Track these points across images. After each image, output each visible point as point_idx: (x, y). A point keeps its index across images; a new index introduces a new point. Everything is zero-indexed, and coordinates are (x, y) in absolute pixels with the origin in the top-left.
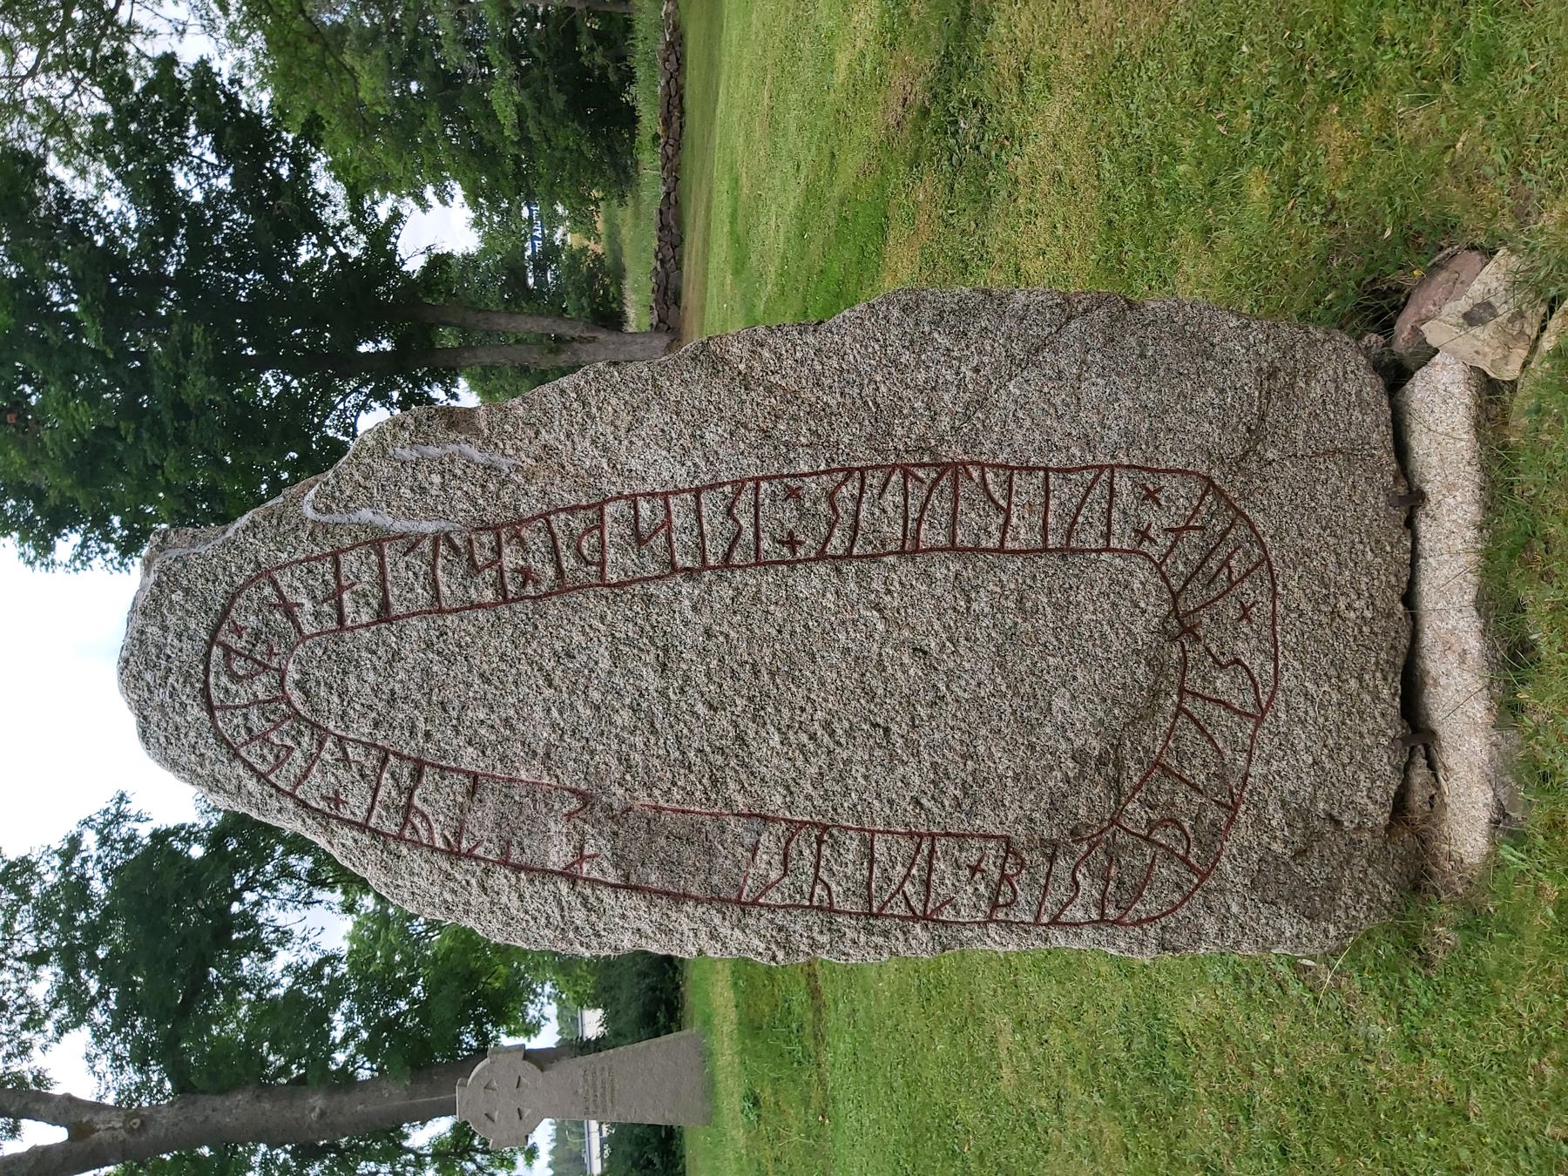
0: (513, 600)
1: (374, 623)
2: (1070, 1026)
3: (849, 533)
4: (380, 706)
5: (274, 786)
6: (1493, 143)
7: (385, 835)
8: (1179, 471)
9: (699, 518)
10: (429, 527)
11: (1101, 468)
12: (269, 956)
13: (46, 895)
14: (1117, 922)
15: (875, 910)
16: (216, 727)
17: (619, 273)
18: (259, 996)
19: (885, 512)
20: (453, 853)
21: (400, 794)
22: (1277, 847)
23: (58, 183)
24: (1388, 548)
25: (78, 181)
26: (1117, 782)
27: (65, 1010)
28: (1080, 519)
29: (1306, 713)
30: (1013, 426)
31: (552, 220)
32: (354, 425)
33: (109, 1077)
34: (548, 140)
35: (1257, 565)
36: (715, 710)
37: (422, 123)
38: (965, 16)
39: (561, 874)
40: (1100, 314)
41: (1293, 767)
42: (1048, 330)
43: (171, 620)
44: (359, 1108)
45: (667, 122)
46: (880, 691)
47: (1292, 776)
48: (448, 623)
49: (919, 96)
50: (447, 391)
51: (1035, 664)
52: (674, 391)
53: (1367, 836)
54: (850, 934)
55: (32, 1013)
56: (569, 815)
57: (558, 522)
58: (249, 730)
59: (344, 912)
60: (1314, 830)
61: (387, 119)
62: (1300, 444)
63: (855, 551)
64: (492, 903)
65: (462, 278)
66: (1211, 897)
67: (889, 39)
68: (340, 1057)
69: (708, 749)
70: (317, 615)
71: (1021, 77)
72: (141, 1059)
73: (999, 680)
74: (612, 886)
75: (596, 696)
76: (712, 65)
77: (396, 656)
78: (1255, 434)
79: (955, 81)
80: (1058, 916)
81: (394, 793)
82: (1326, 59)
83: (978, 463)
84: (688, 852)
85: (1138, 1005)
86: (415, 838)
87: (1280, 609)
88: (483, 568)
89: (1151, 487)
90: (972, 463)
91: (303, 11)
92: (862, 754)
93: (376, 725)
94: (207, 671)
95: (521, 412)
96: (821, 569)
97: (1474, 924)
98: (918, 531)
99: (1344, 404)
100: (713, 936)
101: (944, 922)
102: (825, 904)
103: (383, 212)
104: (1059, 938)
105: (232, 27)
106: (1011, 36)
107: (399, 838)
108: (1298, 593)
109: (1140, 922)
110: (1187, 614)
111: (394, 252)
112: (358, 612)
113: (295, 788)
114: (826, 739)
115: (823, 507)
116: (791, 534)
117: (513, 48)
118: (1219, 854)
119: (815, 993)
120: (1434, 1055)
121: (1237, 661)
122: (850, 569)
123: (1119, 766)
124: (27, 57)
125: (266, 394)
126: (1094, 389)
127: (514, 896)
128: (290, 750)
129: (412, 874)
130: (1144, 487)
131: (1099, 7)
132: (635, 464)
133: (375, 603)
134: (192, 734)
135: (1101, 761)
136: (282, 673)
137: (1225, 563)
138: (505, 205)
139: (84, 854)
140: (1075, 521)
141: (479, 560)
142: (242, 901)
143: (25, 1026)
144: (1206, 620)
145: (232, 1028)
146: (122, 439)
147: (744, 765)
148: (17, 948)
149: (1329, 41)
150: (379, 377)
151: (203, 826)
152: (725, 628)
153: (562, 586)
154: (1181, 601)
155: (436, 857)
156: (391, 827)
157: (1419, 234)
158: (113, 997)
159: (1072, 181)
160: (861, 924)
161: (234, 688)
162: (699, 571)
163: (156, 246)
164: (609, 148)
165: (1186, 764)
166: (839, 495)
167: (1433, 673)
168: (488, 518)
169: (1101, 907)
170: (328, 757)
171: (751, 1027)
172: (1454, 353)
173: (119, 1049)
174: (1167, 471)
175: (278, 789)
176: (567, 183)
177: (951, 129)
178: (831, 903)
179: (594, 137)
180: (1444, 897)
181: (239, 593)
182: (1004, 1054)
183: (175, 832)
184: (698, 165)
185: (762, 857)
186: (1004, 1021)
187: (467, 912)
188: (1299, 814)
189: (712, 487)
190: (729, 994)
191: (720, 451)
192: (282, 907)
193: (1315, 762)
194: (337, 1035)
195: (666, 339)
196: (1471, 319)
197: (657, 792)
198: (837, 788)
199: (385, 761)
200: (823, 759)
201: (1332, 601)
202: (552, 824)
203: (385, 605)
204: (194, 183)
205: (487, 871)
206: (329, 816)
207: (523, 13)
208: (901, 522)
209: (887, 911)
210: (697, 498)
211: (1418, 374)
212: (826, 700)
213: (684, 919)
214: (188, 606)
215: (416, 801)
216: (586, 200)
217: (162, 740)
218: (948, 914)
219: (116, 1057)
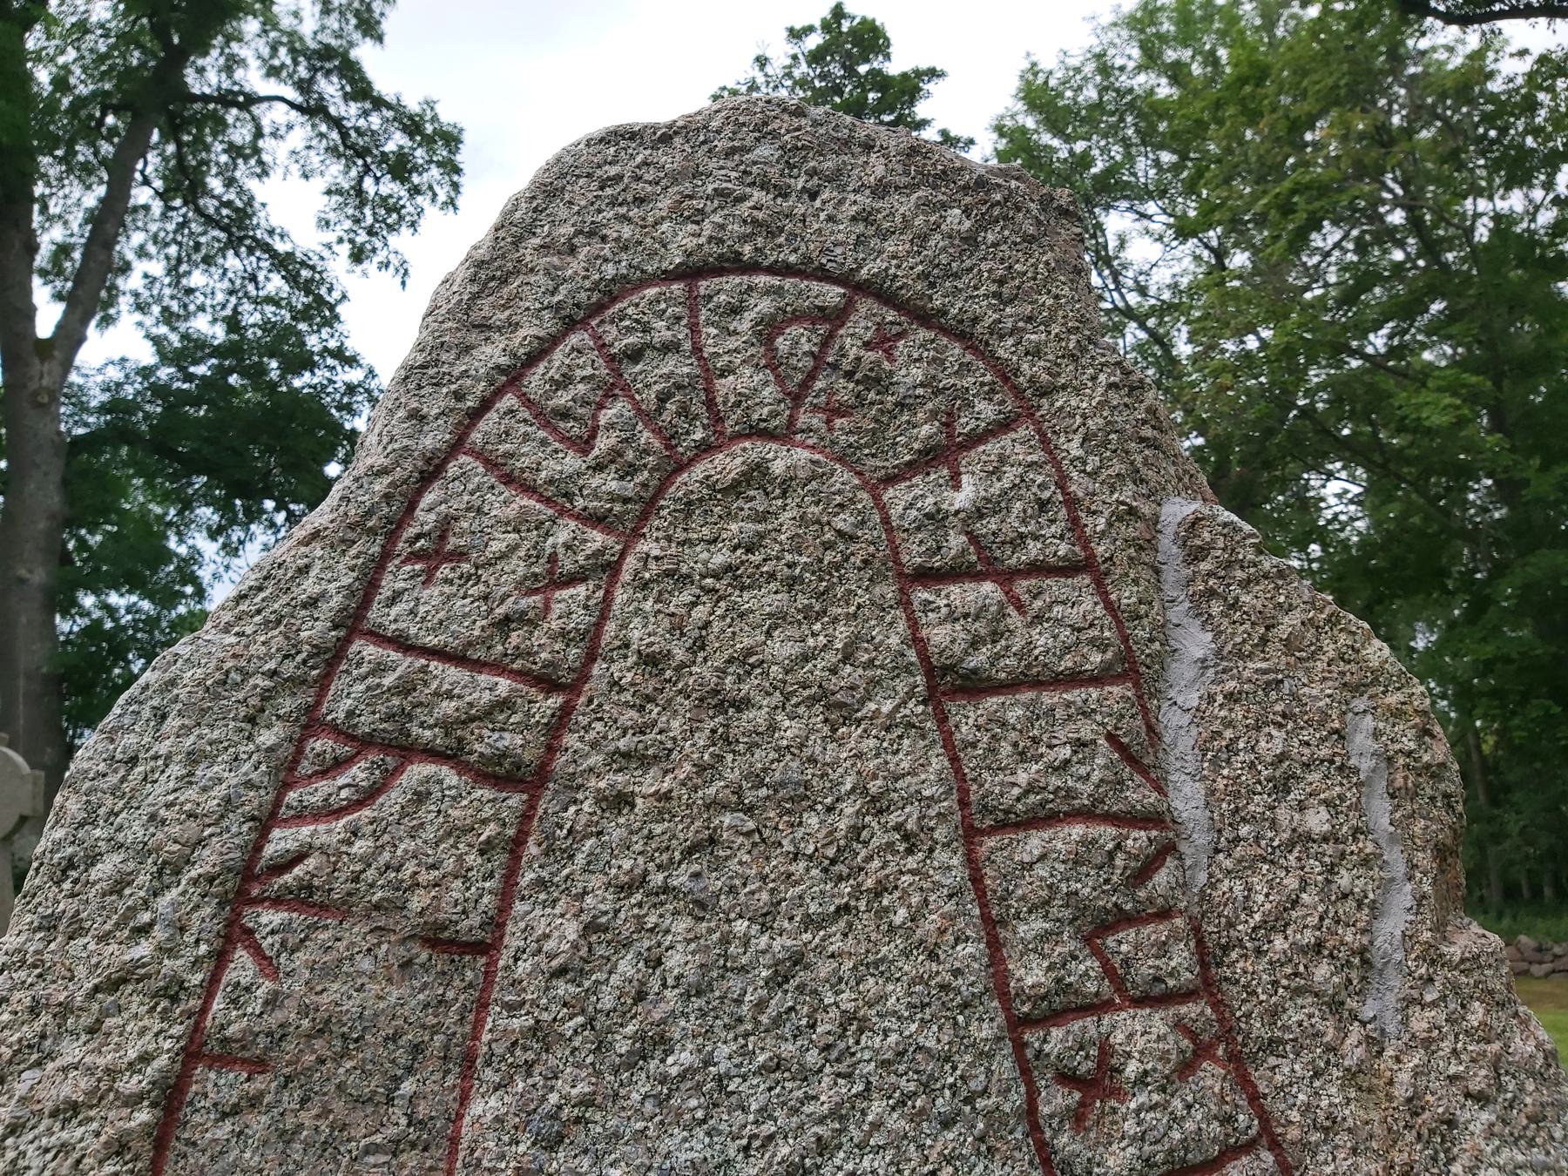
0: (1020, 1046)
1: (924, 657)
4: (703, 671)
5: (486, 405)
10: (1187, 799)
12: (213, 534)
13: (299, 334)
18: (170, 524)
20: (246, 882)
21: (446, 725)
27: (177, 344)
43: (903, 205)
44: (24, 620)
48: (941, 856)
55: (179, 316)
58: (635, 355)
64: (65, 1010)
68: (88, 601)
70: (936, 519)
72: (116, 406)
77: (841, 712)
81: (447, 707)
86: (306, 767)
88: (1097, 953)
93: (651, 661)
94: (785, 270)
107: (311, 722)
112: (952, 617)
113: (478, 455)
127: (74, 1088)
134: (627, 231)
136: (785, 435)
139: (339, 368)
141: (1123, 942)
142: (277, 509)
143: (166, 309)
145: (136, 498)
148: (247, 306)
155: (239, 829)
158: (186, 386)
161: (744, 324)
168: (1240, 966)
170: (562, 536)
181: (973, 349)
187: (49, 925)
194: (114, 599)
199: (547, 682)
203: (975, 686)
205: (173, 991)
214: (936, 240)
215: (418, 771)
217: (613, 171)
219: (119, 385)
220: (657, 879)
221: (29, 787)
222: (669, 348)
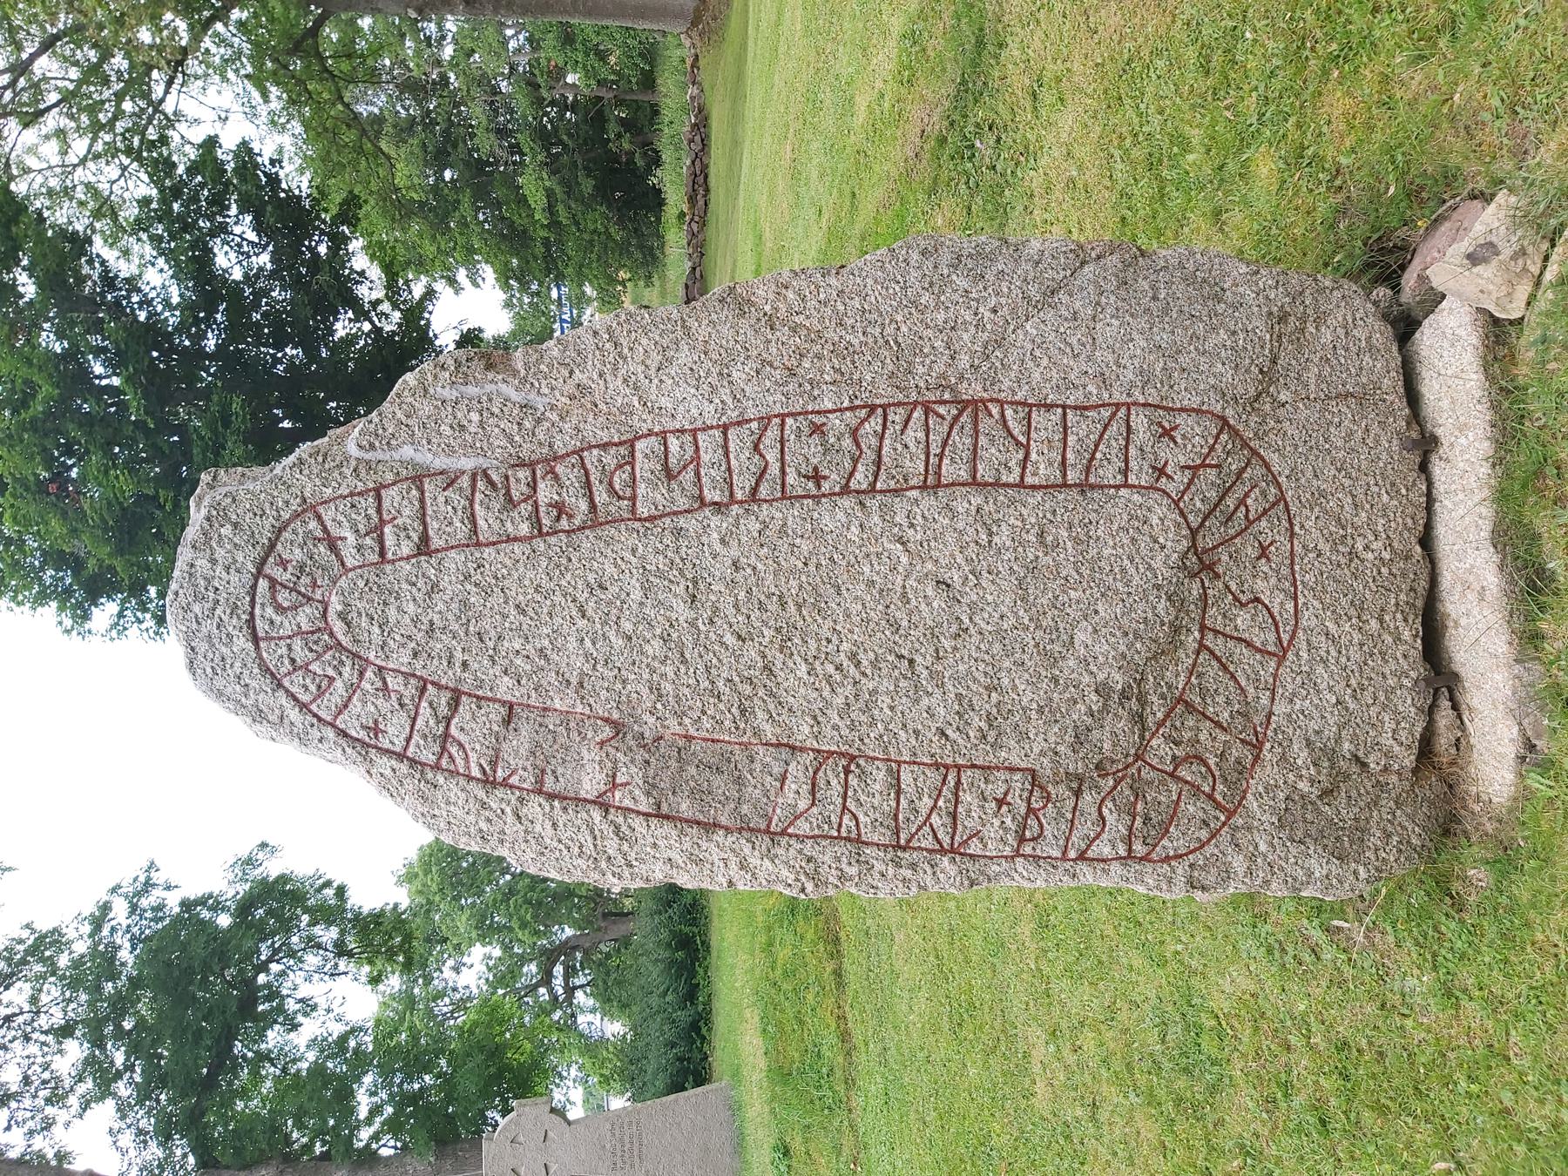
0: (548, 534)
1: (414, 556)
2: (1103, 1028)
3: (873, 468)
5: (315, 715)
6: (1489, 89)
7: (423, 764)
8: (1194, 410)
10: (468, 464)
11: (1118, 406)
14: (1145, 859)
15: (902, 842)
16: (261, 658)
18: (284, 1070)
19: (907, 450)
20: (489, 782)
21: (438, 722)
22: (1303, 786)
23: (103, 263)
24: (1404, 491)
25: (122, 261)
26: (1141, 716)
28: (1098, 455)
29: (1328, 652)
30: (1030, 364)
31: (580, 301)
33: (132, 1153)
34: (577, 224)
35: (1274, 505)
36: (744, 641)
38: (980, 43)
39: (594, 802)
40: (1113, 260)
41: (1317, 706)
42: (1062, 273)
43: (220, 553)
45: (692, 200)
46: (905, 623)
47: (1316, 714)
48: (485, 556)
49: (937, 124)
51: (1056, 598)
52: (702, 332)
53: (1394, 778)
54: (879, 866)
56: (602, 743)
57: (591, 457)
58: (293, 661)
59: (370, 982)
61: (422, 204)
62: (1312, 387)
63: (879, 486)
64: (526, 831)
66: (1239, 835)
67: (907, 78)
68: (365, 1134)
69: (737, 679)
70: (359, 548)
71: (1034, 95)
72: (165, 1135)
73: (1021, 613)
74: (644, 814)
75: (627, 626)
76: (736, 143)
77: (435, 588)
78: (1268, 375)
79: (970, 105)
80: (1085, 852)
81: (432, 722)
82: (1326, 34)
83: (998, 401)
84: (717, 781)
85: (1172, 993)
86: (452, 768)
87: (1298, 549)
89: (1167, 425)
90: (991, 400)
91: (341, 98)
92: (887, 685)
93: (415, 655)
94: (253, 602)
95: (555, 353)
96: (847, 502)
97: (1505, 859)
98: (940, 466)
99: (1354, 349)
100: (743, 866)
101: (971, 856)
102: (853, 835)
103: (418, 290)
104: (1087, 875)
105: (271, 113)
106: (1024, 57)
107: (437, 767)
108: (1315, 534)
109: (1167, 859)
110: (1206, 551)
112: (399, 545)
114: (852, 670)
115: (847, 442)
116: (816, 469)
117: (545, 138)
118: (1245, 792)
119: (845, 1036)
120: (1471, 999)
121: (1257, 600)
122: (873, 503)
123: (1143, 701)
124: (80, 146)
126: (1109, 329)
127: (548, 825)
128: (331, 680)
129: (448, 803)
130: (1160, 424)
131: (1110, 18)
132: (664, 402)
135: (1124, 695)
137: (1242, 502)
138: (534, 287)
139: (113, 923)
140: (1093, 458)
142: (267, 971)
143: (48, 1101)
144: (1225, 558)
146: (161, 507)
147: (772, 695)
148: (43, 1021)
149: (1329, 16)
151: (229, 896)
153: (595, 521)
154: (1199, 538)
157: (1422, 188)
158: (138, 1070)
159: (1085, 186)
160: (889, 856)
161: (278, 619)
162: (727, 506)
163: (197, 322)
164: (636, 230)
165: (1209, 701)
166: (861, 431)
167: (1453, 615)
168: (525, 454)
171: (781, 1074)
172: (1459, 295)
173: (143, 1123)
174: (1182, 410)
175: (320, 719)
177: (967, 153)
178: (859, 835)
179: (621, 222)
180: (1474, 839)
182: (1037, 1069)
183: (202, 901)
184: (722, 240)
185: (791, 786)
186: (1037, 1034)
188: (1325, 754)
189: (739, 423)
190: (758, 1041)
191: (747, 389)
192: (308, 979)
193: (1338, 702)
194: (363, 1113)
196: (1473, 259)
197: (687, 721)
198: (863, 718)
199: (423, 690)
200: (849, 690)
201: (1350, 542)
202: (585, 752)
203: (425, 538)
204: (234, 261)
205: (521, 800)
206: (369, 746)
207: (553, 103)
208: (923, 457)
209: (915, 844)
210: (725, 434)
211: (1426, 323)
212: (851, 632)
213: (716, 848)
215: (453, 731)
216: (613, 281)
217: (209, 670)
218: (974, 847)
219: (140, 1132)
220: (491, 652)
221: (527, 1109)
222: (289, 647)
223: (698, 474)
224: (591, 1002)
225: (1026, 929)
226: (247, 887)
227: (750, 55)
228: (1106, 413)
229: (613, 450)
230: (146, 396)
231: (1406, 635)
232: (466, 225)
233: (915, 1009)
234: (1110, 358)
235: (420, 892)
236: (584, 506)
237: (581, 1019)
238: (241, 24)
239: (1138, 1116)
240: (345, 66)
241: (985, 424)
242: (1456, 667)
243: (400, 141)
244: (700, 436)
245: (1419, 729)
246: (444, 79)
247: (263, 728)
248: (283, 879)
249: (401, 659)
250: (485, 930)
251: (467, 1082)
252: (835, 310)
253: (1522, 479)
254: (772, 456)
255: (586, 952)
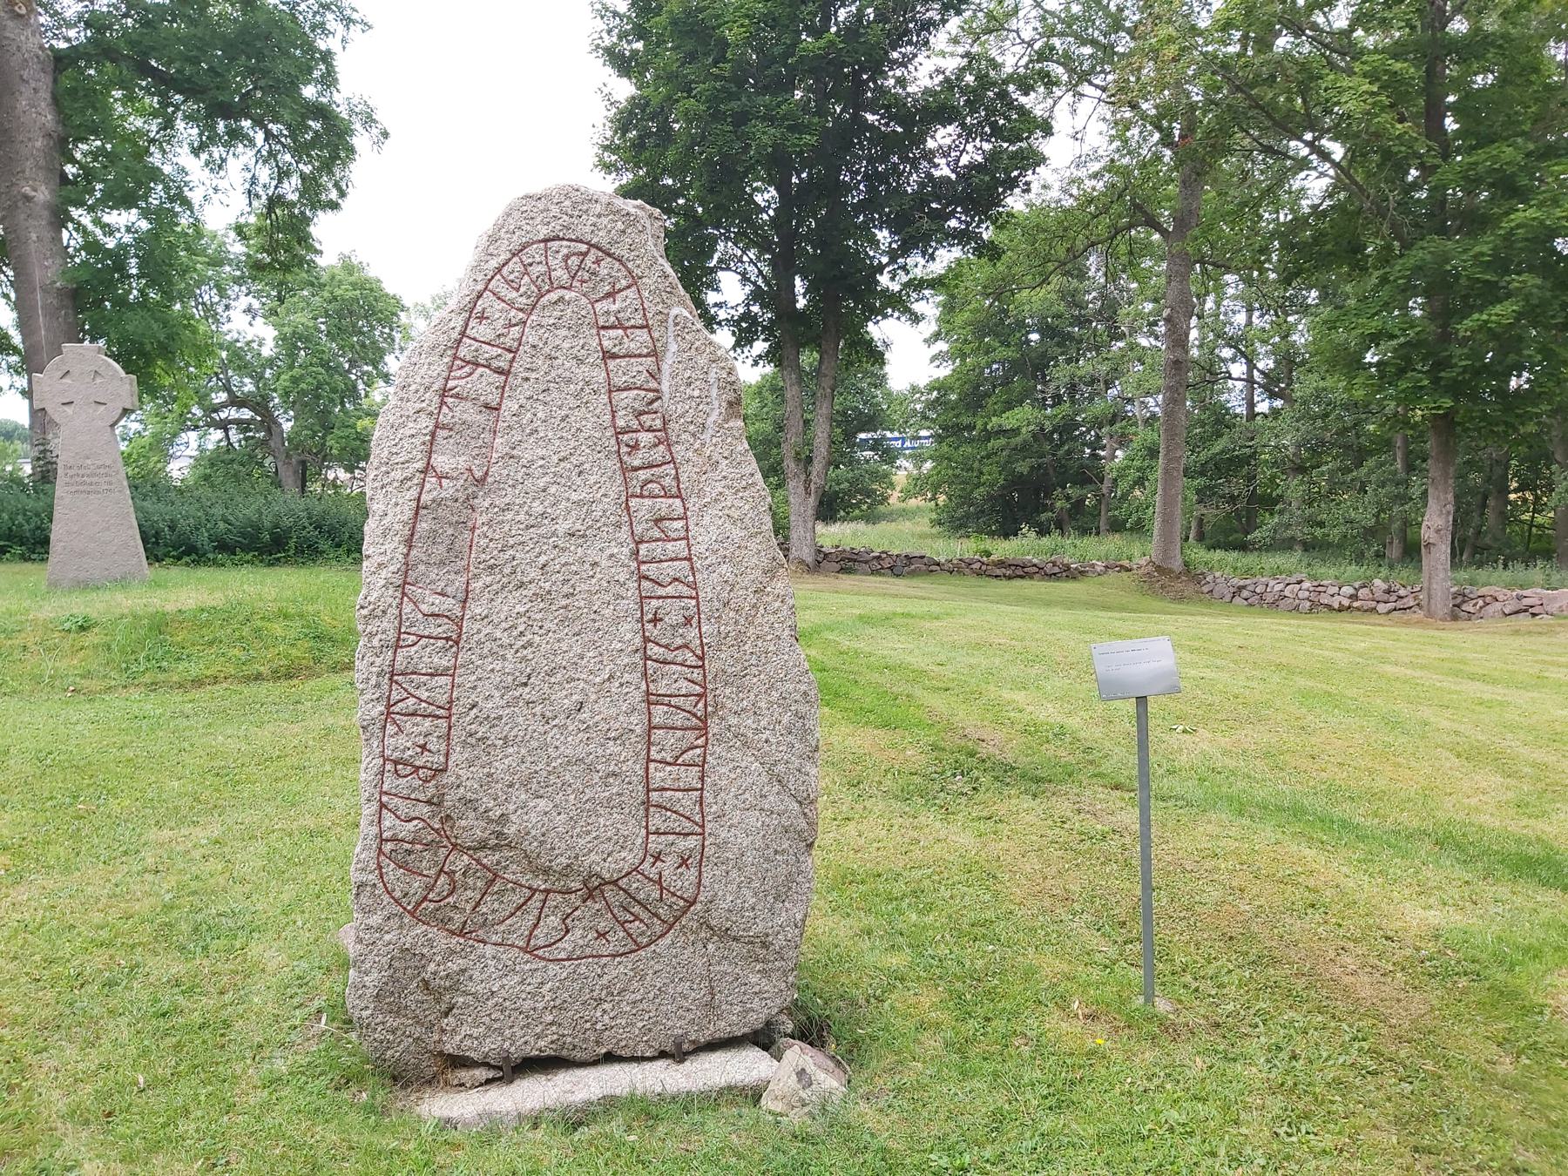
4: (547, 350)
9: (672, 560)
10: (665, 387)
11: (703, 826)
12: (196, 152)
17: (871, 518)
18: (153, 141)
20: (444, 392)
22: (432, 967)
31: (918, 459)
32: (728, 269)
34: (988, 456)
37: (1002, 343)
38: (1038, 780)
43: (605, 220)
44: (34, 236)
45: (1001, 564)
47: (484, 976)
49: (983, 750)
50: (760, 357)
52: (753, 545)
53: (436, 1038)
56: (470, 470)
60: (442, 995)
61: (1006, 312)
65: (865, 373)
75: (553, 490)
76: (1049, 604)
77: (580, 362)
78: (725, 934)
84: (442, 549)
87: (604, 960)
92: (509, 667)
95: (740, 448)
96: (638, 640)
104: (369, 810)
107: (455, 357)
109: (380, 868)
111: (885, 316)
115: (679, 641)
117: (1067, 428)
119: (198, 683)
122: (637, 658)
125: (756, 189)
126: (754, 819)
127: (413, 432)
128: (518, 290)
132: (707, 519)
133: (615, 350)
135: (499, 835)
136: (569, 288)
137: (637, 918)
141: (643, 418)
144: (597, 906)
146: (715, 63)
147: (503, 587)
150: (773, 295)
152: (598, 576)
153: (626, 470)
156: (462, 352)
161: (560, 256)
163: (888, 108)
168: (671, 425)
169: (393, 839)
171: (160, 625)
176: (950, 472)
179: (991, 498)
182: (185, 832)
184: (963, 590)
185: (438, 599)
195: (809, 560)
196: (801, 1073)
199: (510, 351)
200: (506, 641)
203: (614, 356)
204: (942, 142)
205: (431, 414)
207: (1098, 437)
209: (394, 686)
215: (481, 370)
216: (936, 488)
218: (391, 729)
223: (658, 540)
224: (211, 446)
225: (310, 822)
226: (344, 115)
227: (1101, 614)
228: (697, 818)
229: (674, 483)
230: (817, 57)
231: (542, 1043)
232: (987, 353)
233: (228, 740)
234: (735, 821)
235: (333, 277)
236: (637, 463)
237: (193, 435)
238: (1158, 158)
239: (153, 900)
240: (1123, 248)
241: (691, 735)
242: (517, 1082)
243: (1063, 294)
244: (684, 542)
245: (472, 1055)
246: (1122, 337)
247: (484, 242)
248: (351, 150)
249: (531, 337)
250: (290, 342)
251: (128, 313)
252: (768, 633)
253: (647, 1110)
254: (670, 590)
255: (263, 443)
